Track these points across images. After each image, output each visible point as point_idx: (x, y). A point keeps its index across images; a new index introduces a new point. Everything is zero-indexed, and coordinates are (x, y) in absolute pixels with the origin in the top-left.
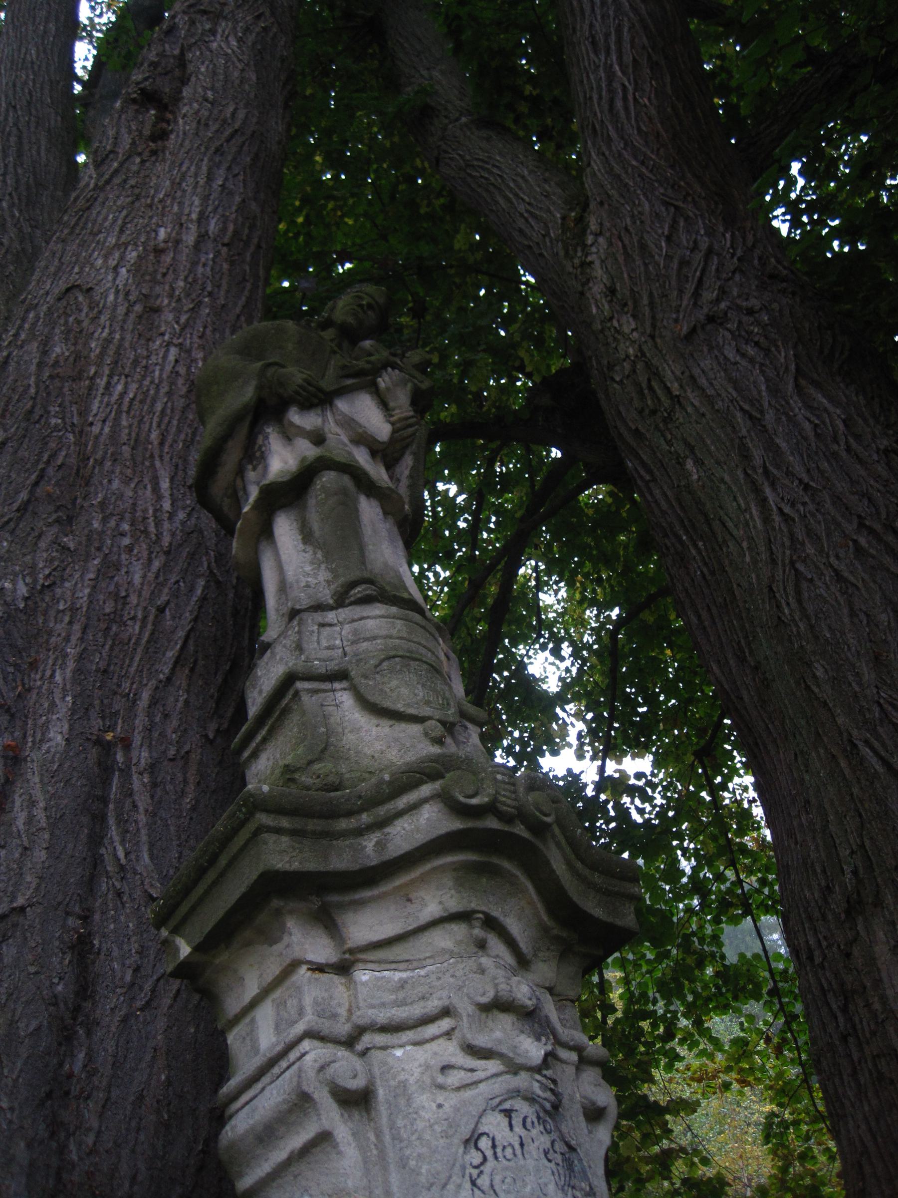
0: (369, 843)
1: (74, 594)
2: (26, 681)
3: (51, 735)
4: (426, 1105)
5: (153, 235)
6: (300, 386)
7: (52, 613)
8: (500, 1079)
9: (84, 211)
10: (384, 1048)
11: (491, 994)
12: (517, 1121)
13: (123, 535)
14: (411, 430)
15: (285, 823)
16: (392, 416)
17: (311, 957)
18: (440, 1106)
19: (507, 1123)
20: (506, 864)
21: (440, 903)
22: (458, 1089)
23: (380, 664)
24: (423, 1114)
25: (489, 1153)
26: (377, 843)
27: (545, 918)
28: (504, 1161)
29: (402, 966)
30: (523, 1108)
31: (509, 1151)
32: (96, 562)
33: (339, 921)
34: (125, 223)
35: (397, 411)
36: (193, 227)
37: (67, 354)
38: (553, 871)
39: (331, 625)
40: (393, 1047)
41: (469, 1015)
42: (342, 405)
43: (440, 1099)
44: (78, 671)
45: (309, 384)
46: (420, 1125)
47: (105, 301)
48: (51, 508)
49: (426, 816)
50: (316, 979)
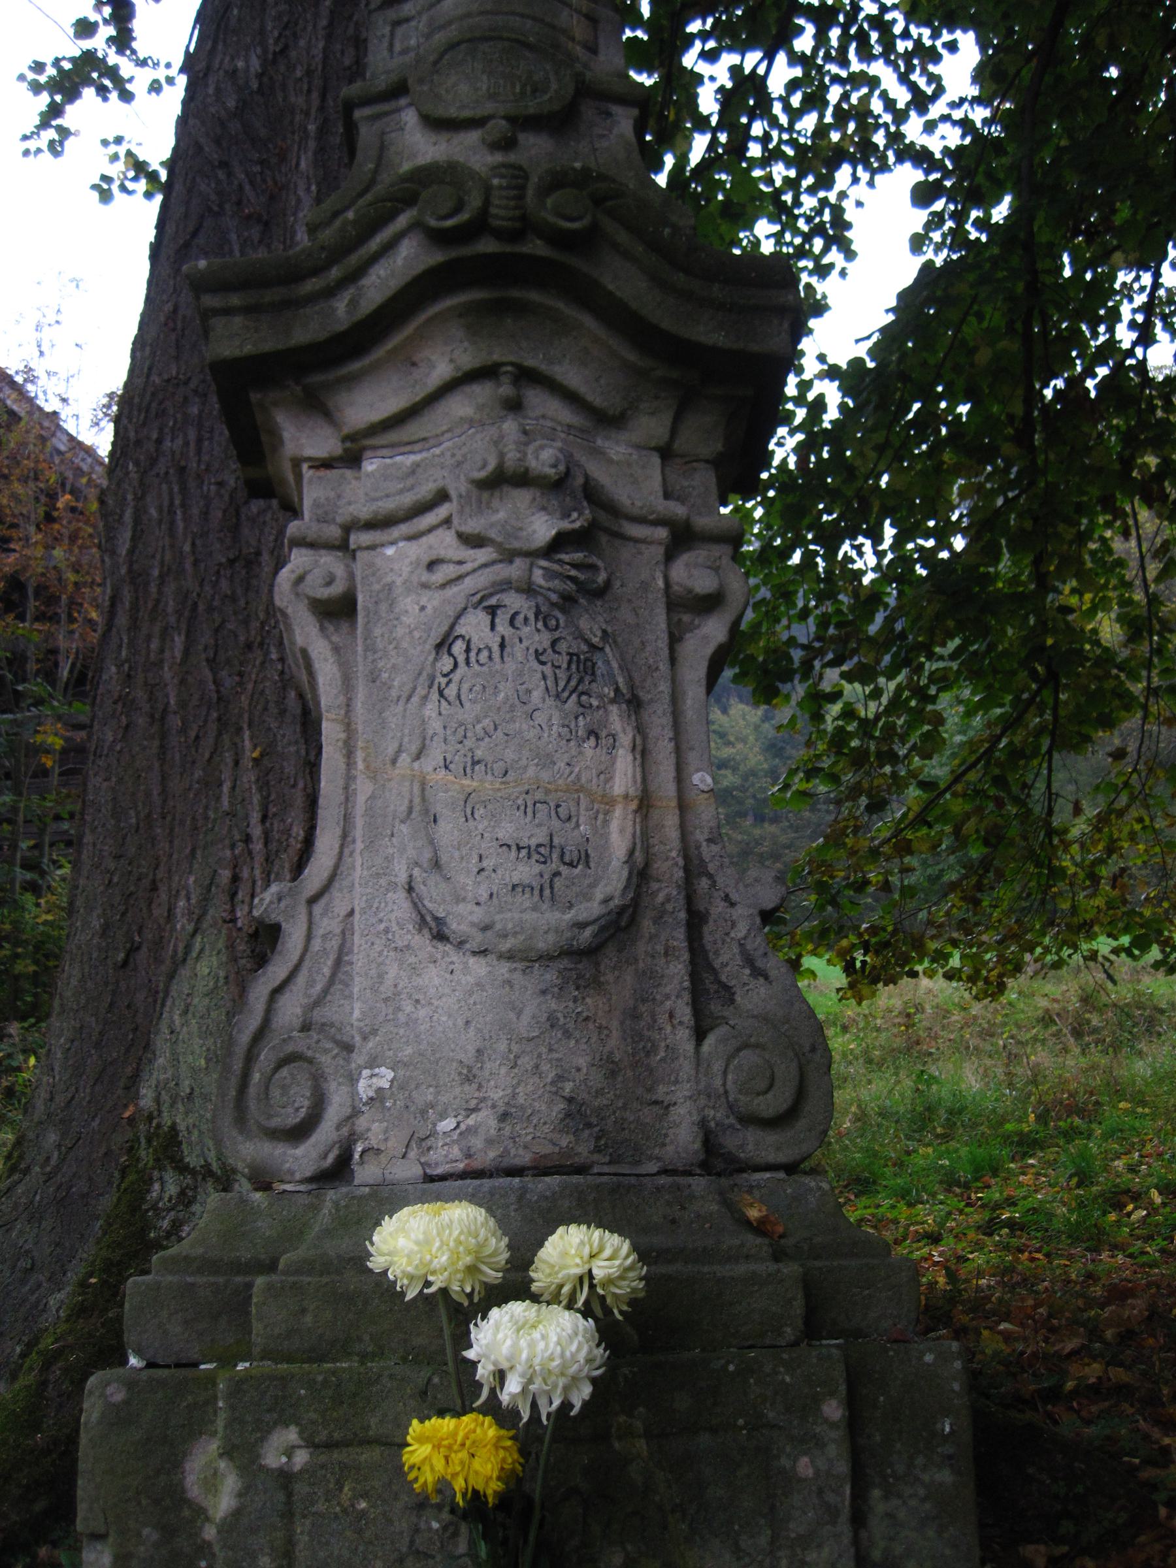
0: (340, 305)
4: (409, 608)
11: (492, 465)
12: (502, 619)
15: (235, 300)
17: (309, 452)
18: (423, 608)
19: (488, 622)
20: (534, 296)
22: (443, 586)
24: (404, 619)
25: (461, 659)
27: (632, 357)
28: (476, 667)
29: (417, 447)
30: (514, 601)
31: (485, 653)
33: (330, 405)
38: (611, 293)
40: (383, 545)
41: (460, 496)
43: (424, 601)
44: (321, 150)
46: (400, 632)
50: (320, 478)
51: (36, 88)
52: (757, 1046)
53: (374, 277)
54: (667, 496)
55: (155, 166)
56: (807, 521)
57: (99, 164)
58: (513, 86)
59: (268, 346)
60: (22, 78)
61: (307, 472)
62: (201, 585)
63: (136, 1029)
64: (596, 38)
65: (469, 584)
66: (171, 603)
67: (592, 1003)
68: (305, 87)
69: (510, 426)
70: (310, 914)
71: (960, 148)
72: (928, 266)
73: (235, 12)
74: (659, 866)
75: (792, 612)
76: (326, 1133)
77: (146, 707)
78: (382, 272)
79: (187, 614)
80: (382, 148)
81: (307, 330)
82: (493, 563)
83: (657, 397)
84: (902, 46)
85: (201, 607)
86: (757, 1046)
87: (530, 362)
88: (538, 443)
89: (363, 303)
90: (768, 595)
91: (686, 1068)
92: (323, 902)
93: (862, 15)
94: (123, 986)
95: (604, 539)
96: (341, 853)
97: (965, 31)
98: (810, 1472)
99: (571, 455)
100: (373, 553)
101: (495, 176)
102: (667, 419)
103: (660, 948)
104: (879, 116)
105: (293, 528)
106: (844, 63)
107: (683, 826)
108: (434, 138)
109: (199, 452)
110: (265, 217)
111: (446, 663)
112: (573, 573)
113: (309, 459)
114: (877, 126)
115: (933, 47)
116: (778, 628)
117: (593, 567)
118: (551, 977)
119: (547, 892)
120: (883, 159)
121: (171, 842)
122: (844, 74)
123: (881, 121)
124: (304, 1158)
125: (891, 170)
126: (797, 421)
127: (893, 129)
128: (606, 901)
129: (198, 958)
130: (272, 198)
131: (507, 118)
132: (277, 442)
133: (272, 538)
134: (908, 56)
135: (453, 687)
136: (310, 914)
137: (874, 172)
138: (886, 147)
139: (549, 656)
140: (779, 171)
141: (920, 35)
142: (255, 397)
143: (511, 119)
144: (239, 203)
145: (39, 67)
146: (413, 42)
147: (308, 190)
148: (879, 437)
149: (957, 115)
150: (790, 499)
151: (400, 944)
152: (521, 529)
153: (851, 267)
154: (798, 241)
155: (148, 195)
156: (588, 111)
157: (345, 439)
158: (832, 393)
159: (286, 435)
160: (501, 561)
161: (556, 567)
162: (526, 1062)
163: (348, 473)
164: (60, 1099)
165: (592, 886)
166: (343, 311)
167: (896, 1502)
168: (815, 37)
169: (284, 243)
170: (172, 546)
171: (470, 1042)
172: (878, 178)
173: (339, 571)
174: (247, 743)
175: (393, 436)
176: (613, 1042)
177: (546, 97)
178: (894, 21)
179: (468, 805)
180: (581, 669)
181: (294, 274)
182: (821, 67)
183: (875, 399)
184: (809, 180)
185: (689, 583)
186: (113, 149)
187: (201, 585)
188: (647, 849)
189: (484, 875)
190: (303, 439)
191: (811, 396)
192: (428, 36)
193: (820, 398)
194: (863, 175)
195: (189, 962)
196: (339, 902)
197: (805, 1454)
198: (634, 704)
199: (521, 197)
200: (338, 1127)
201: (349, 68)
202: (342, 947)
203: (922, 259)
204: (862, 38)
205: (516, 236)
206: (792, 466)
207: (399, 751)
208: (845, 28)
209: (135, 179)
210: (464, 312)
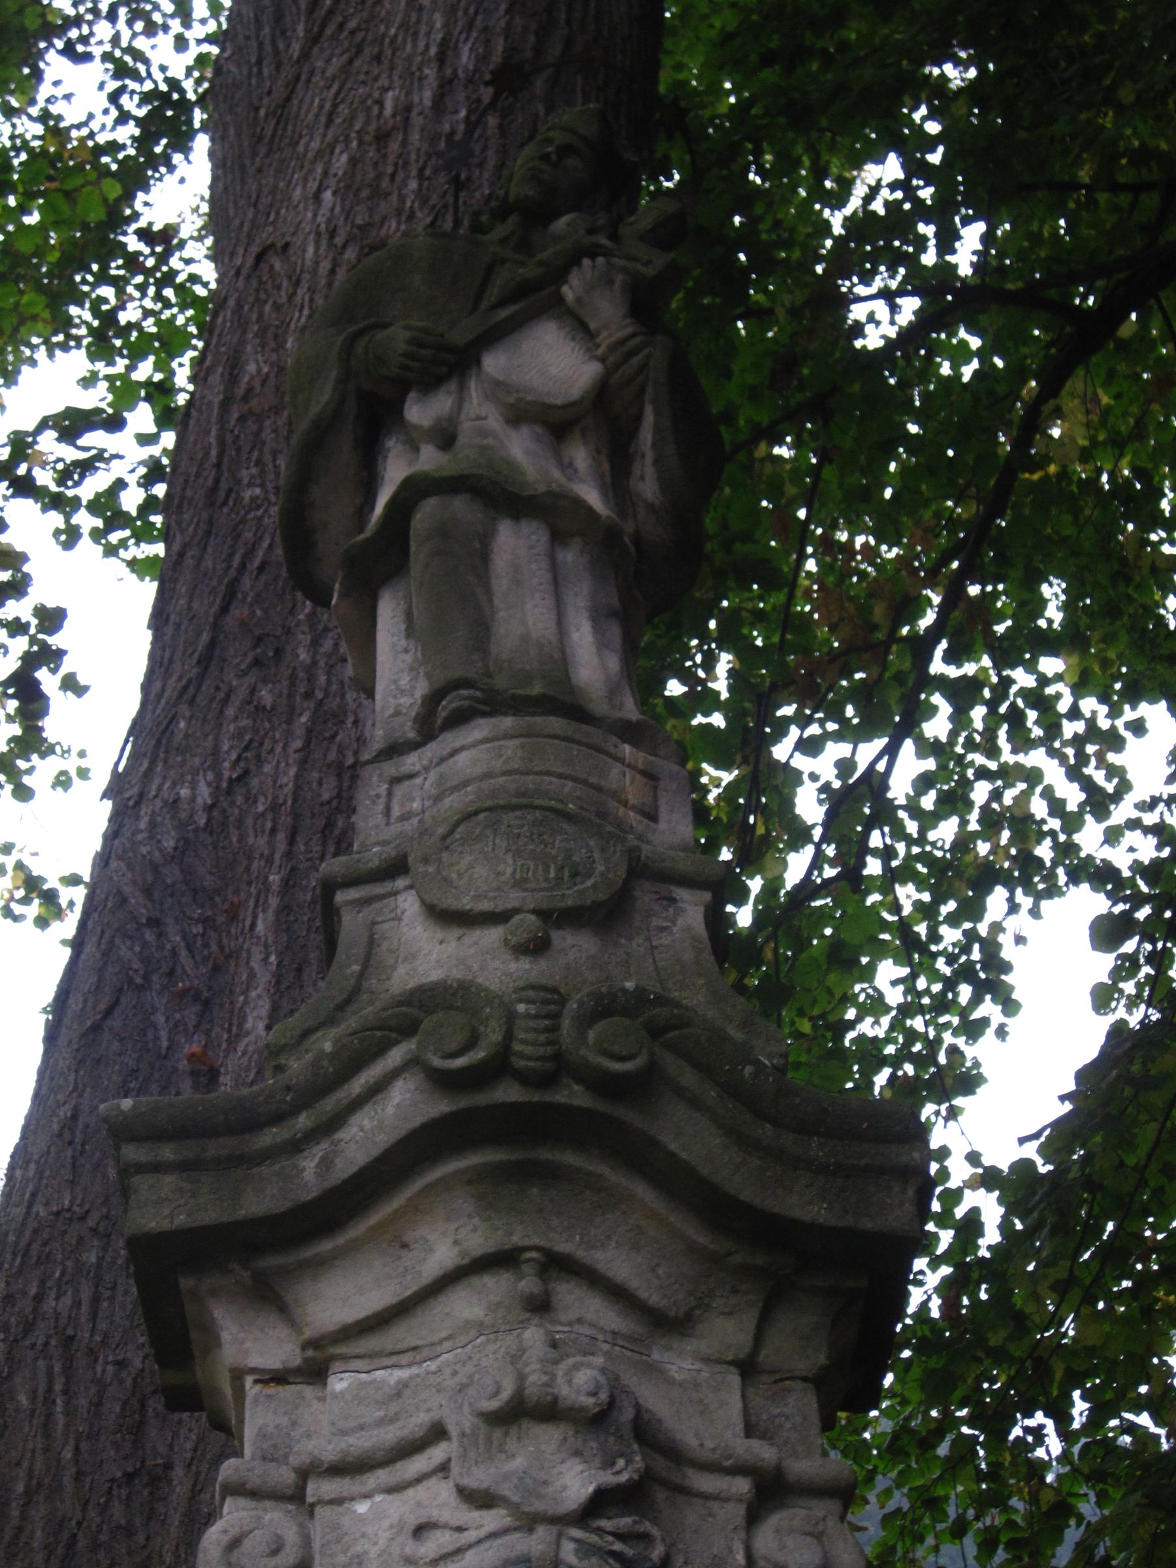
0: (309, 1164)
1: (275, 782)
2: (225, 941)
3: (249, 1025)
5: (375, 110)
6: (406, 355)
7: (249, 821)
8: (499, 1541)
9: (283, 107)
10: (338, 1501)
11: (506, 1394)
14: (635, 361)
15: (167, 1153)
16: (598, 346)
17: (255, 1361)
20: (570, 1158)
21: (456, 1243)
23: (451, 832)
26: (323, 1160)
27: (702, 1238)
29: (405, 1359)
32: (303, 719)
34: (335, 106)
35: (605, 334)
36: (430, 72)
37: (266, 370)
38: (673, 1155)
39: (410, 776)
40: (352, 1499)
41: (463, 1434)
42: (493, 363)
44: (285, 909)
45: (421, 345)
47: (304, 260)
49: (396, 1101)
50: (269, 1397)
53: (355, 1130)
54: (750, 1430)
56: (958, 1394)
58: (547, 870)
59: (208, 1217)
62: (84, 1509)
64: (656, 798)
66: (39, 1533)
68: (269, 825)
69: (533, 1335)
71: (1156, 863)
72: (1118, 1031)
73: (182, 725)
75: (940, 1527)
78: (366, 1123)
79: (60, 1551)
80: (372, 943)
81: (261, 1199)
82: (506, 1531)
83: (735, 1291)
84: (1070, 729)
85: (81, 1543)
87: (563, 1247)
88: (571, 1361)
89: (339, 1163)
90: (906, 1505)
93: (1014, 689)
95: (660, 1495)
97: (1153, 701)
99: (617, 1378)
100: (340, 1509)
101: (521, 1001)
102: (750, 1321)
104: (1043, 821)
105: (228, 1469)
106: (992, 751)
108: (440, 935)
110: (206, 994)
112: (618, 1546)
113: (254, 1370)
114: (1041, 836)
115: (1113, 728)
116: (920, 1552)
117: (645, 1537)
120: (1050, 877)
122: (993, 766)
123: (1045, 828)
125: (1061, 894)
126: (941, 1248)
127: (1062, 838)
130: (216, 969)
131: (537, 912)
132: (212, 1341)
133: (189, 1445)
134: (1078, 741)
137: (1039, 897)
138: (1055, 863)
140: (907, 895)
141: (1094, 713)
142: (186, 1283)
143: (543, 914)
144: (171, 973)
146: (416, 805)
147: (265, 960)
148: (1060, 1272)
149: (1150, 819)
150: (935, 1363)
152: (545, 1483)
153: (1012, 1023)
154: (937, 988)
156: (644, 895)
157: (305, 1346)
158: (990, 1208)
159: (225, 1336)
160: (516, 1529)
161: (593, 1538)
163: (308, 1391)
166: (310, 1173)
168: (951, 718)
169: (229, 1031)
170: (46, 1450)
172: (1045, 905)
173: (291, 1535)
177: (589, 883)
178: (1058, 696)
182: (961, 757)
183: (1050, 1219)
184: (951, 906)
187: (84, 1509)
190: (248, 1342)
191: (959, 1212)
192: (437, 799)
193: (974, 1212)
194: (1025, 902)
199: (554, 1029)
201: (328, 802)
203: (1111, 1019)
204: (1016, 718)
205: (545, 1081)
206: (935, 1313)
208: (993, 705)
209: (26, 901)
210: (474, 1177)
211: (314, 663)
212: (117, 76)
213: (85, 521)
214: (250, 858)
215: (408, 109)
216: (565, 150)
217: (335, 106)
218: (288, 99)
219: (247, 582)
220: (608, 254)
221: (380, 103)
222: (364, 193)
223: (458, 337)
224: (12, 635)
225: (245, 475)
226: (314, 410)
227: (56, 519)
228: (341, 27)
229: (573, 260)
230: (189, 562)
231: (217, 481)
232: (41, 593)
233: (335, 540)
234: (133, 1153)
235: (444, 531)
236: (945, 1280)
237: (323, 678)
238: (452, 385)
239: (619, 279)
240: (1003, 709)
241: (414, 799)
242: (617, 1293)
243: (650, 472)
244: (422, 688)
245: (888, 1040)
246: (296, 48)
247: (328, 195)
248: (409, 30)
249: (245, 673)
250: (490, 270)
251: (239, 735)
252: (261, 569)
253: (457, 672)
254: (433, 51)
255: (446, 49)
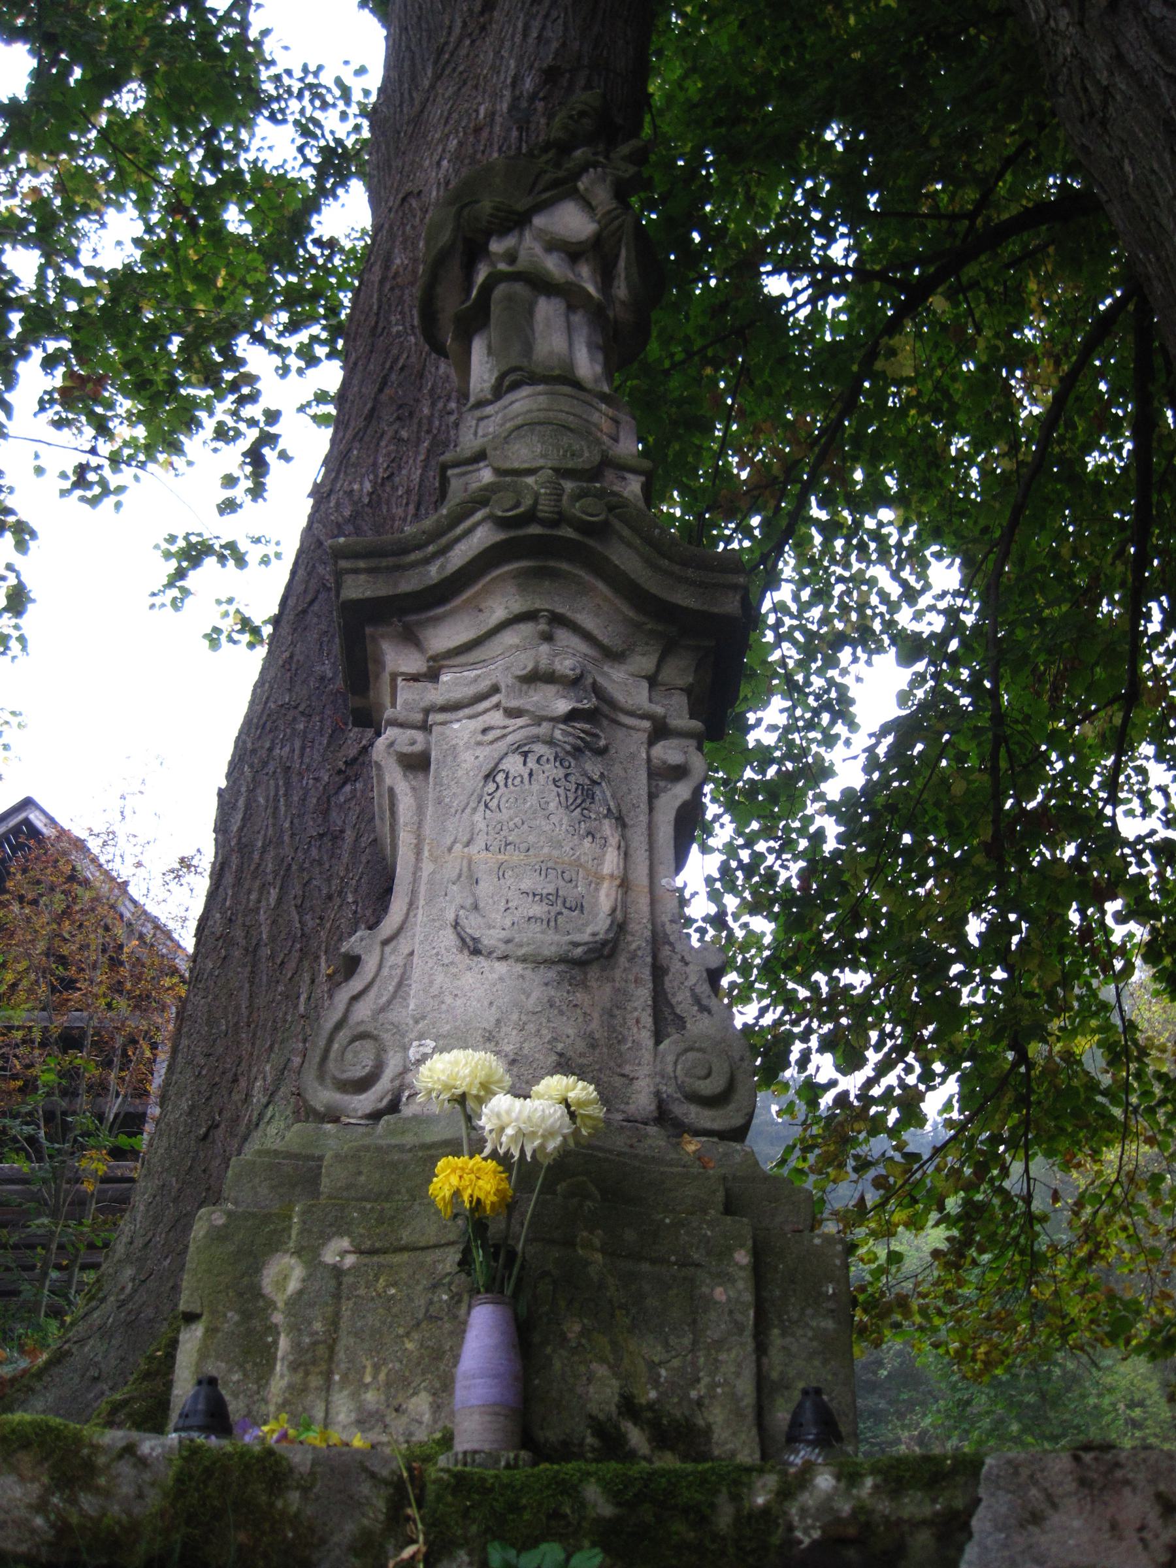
6: (491, 215)
7: (393, 500)
11: (530, 667)
13: (450, 413)
14: (616, 223)
15: (362, 564)
17: (403, 669)
20: (565, 566)
22: (492, 742)
25: (502, 784)
27: (631, 614)
30: (540, 749)
34: (450, 114)
36: (507, 93)
38: (616, 566)
39: (488, 417)
42: (539, 221)
46: (460, 773)
48: (394, 407)
51: (168, 555)
52: (700, 1050)
54: (651, 701)
55: (257, 622)
57: (212, 617)
60: (157, 547)
61: (400, 682)
63: (208, 1189)
65: (510, 739)
67: (580, 996)
69: (545, 648)
70: (382, 952)
74: (633, 926)
76: (384, 1084)
77: (243, 942)
81: (409, 584)
85: (294, 867)
86: (700, 1050)
91: (647, 1056)
92: (394, 943)
94: (202, 1154)
95: (605, 723)
96: (407, 914)
98: (724, 1298)
103: (631, 977)
106: (847, 566)
107: (653, 912)
109: (302, 755)
111: (491, 787)
113: (402, 674)
114: (875, 615)
118: (551, 974)
119: (552, 924)
121: (253, 1044)
122: (847, 574)
124: (365, 1102)
127: (887, 617)
128: (594, 934)
129: (268, 1123)
132: (380, 663)
135: (495, 801)
136: (382, 952)
137: (871, 653)
138: (882, 632)
139: (563, 782)
142: (368, 630)
145: (172, 539)
149: (942, 605)
151: (446, 961)
154: (808, 715)
155: (251, 645)
158: (832, 828)
162: (531, 1028)
163: (429, 685)
164: (139, 1242)
165: (586, 925)
166: (434, 572)
167: (789, 1339)
170: (274, 825)
171: (491, 1015)
172: (875, 657)
174: (323, 964)
175: (462, 659)
176: (595, 1025)
178: (890, 535)
179: (501, 871)
180: (585, 794)
181: (404, 549)
182: (826, 569)
185: (665, 757)
186: (225, 607)
188: (625, 914)
189: (508, 907)
190: (399, 660)
194: (864, 657)
195: (262, 1125)
196: (404, 945)
197: (720, 1285)
198: (621, 822)
200: (392, 1081)
202: (403, 974)
204: (862, 548)
205: (554, 524)
207: (454, 842)
211: (432, 415)
212: (303, 135)
213: (294, 362)
214: (393, 520)
215: (493, 114)
216: (582, 114)
217: (450, 114)
218: (422, 111)
219: (393, 377)
220: (604, 167)
221: (477, 111)
222: (467, 161)
223: (520, 207)
224: (249, 426)
225: (393, 319)
226: (440, 244)
227: (276, 360)
228: (454, 70)
229: (584, 169)
230: (360, 367)
231: (377, 323)
232: (265, 402)
233: (450, 305)
234: (343, 564)
235: (510, 298)
236: (802, 870)
237: (437, 423)
238: (516, 233)
239: (609, 179)
240: (855, 542)
241: (490, 428)
242: (587, 636)
243: (623, 285)
244: (496, 374)
245: (776, 748)
246: (426, 83)
247: (445, 163)
248: (495, 69)
249: (391, 424)
250: (538, 176)
251: (389, 454)
252: (402, 369)
253: (514, 363)
254: (509, 81)
255: (516, 81)
